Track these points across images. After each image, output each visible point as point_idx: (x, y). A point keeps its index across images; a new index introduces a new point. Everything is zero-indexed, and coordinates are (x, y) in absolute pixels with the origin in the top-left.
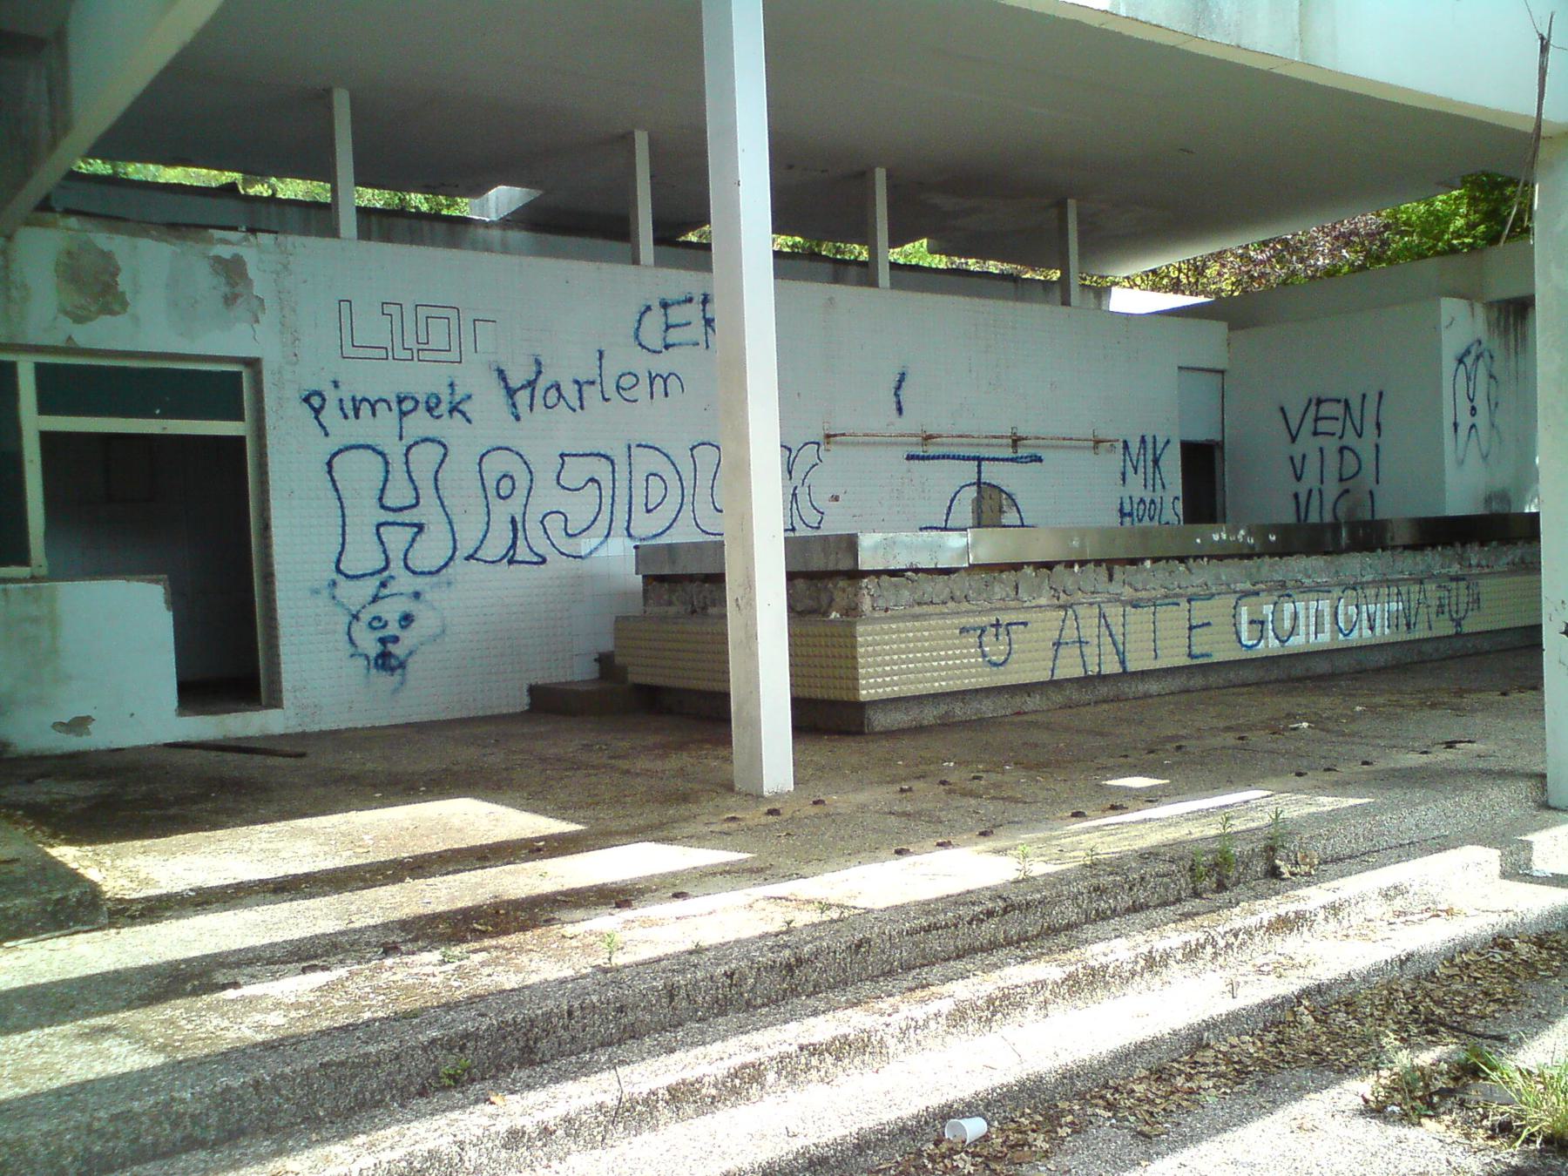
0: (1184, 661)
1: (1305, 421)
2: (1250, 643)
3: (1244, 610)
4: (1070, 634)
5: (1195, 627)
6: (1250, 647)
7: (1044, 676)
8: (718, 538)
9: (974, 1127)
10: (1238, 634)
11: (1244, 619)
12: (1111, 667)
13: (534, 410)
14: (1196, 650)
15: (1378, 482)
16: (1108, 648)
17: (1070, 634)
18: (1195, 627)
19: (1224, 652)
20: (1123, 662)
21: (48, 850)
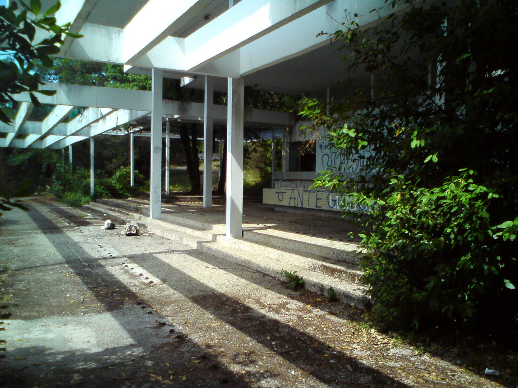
0: (314, 207)
1: (6, 55)
2: (332, 206)
3: (331, 196)
4: (293, 196)
5: (319, 199)
6: (332, 207)
7: (287, 205)
8: (168, 124)
9: (105, 215)
10: (328, 202)
11: (331, 199)
12: (300, 206)
13: (128, 237)
14: (318, 205)
15: (382, 8)
16: (299, 201)
17: (293, 196)
18: (319, 199)
19: (325, 207)
20: (302, 205)
21: (440, 188)
